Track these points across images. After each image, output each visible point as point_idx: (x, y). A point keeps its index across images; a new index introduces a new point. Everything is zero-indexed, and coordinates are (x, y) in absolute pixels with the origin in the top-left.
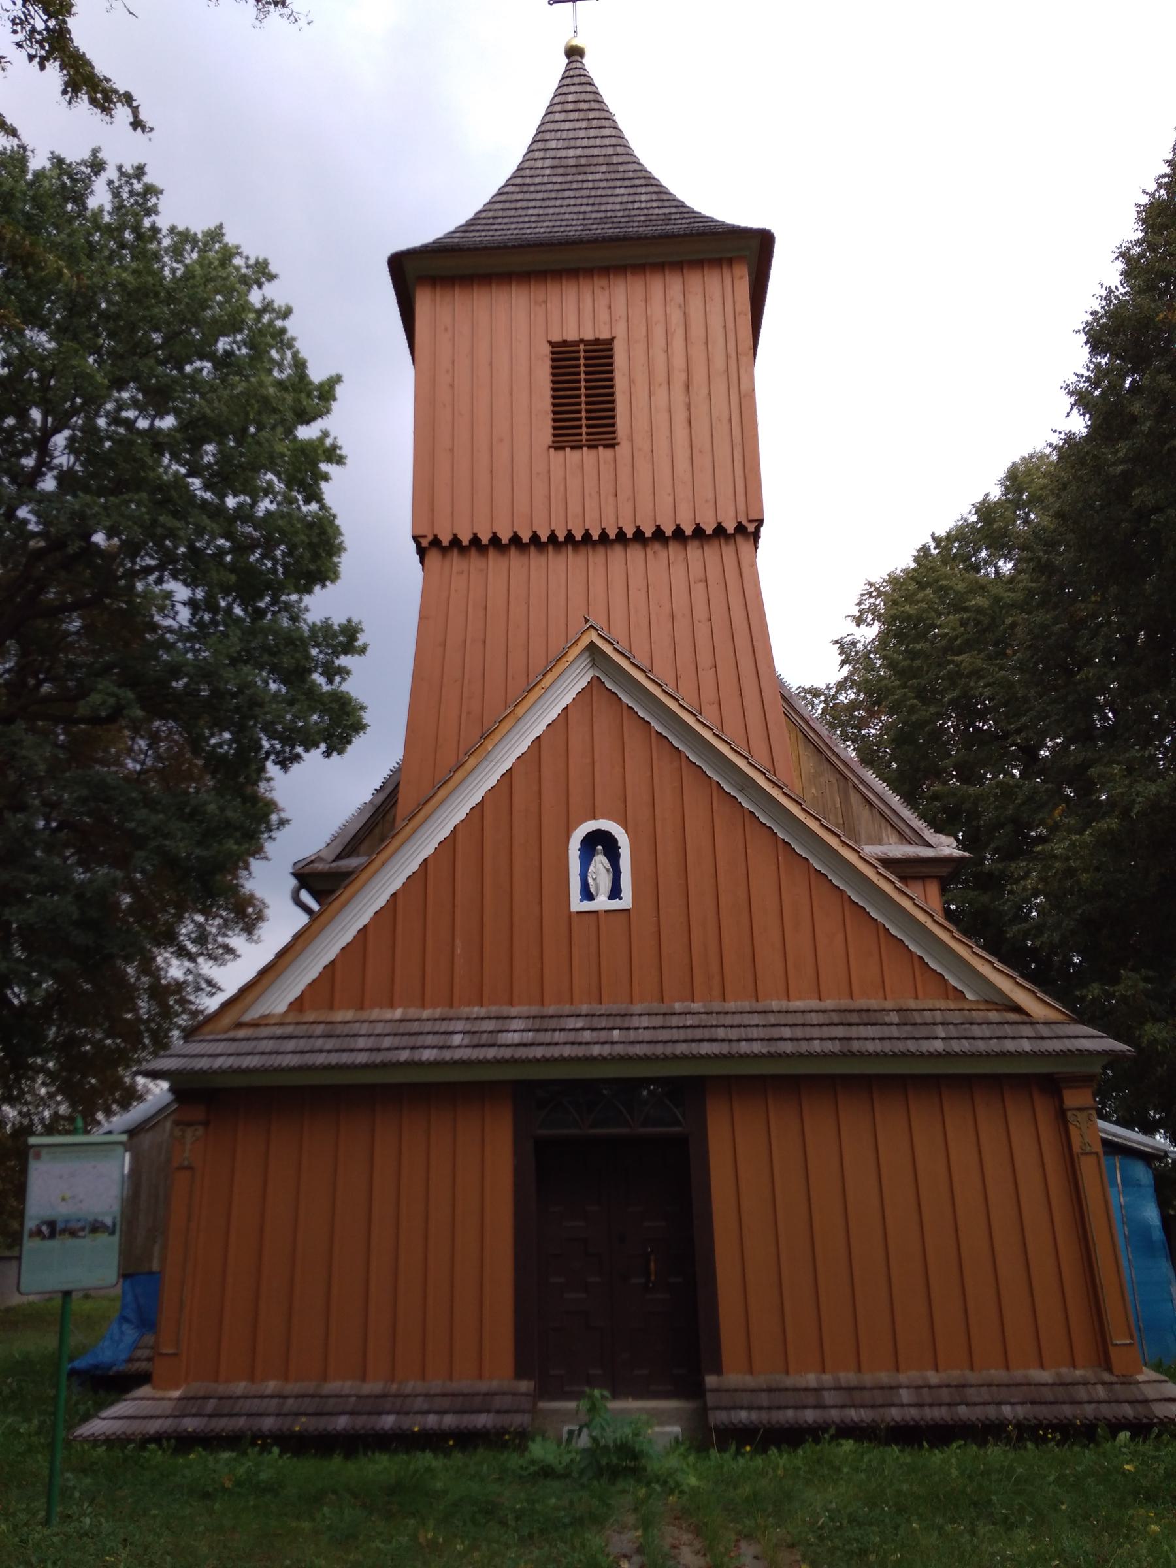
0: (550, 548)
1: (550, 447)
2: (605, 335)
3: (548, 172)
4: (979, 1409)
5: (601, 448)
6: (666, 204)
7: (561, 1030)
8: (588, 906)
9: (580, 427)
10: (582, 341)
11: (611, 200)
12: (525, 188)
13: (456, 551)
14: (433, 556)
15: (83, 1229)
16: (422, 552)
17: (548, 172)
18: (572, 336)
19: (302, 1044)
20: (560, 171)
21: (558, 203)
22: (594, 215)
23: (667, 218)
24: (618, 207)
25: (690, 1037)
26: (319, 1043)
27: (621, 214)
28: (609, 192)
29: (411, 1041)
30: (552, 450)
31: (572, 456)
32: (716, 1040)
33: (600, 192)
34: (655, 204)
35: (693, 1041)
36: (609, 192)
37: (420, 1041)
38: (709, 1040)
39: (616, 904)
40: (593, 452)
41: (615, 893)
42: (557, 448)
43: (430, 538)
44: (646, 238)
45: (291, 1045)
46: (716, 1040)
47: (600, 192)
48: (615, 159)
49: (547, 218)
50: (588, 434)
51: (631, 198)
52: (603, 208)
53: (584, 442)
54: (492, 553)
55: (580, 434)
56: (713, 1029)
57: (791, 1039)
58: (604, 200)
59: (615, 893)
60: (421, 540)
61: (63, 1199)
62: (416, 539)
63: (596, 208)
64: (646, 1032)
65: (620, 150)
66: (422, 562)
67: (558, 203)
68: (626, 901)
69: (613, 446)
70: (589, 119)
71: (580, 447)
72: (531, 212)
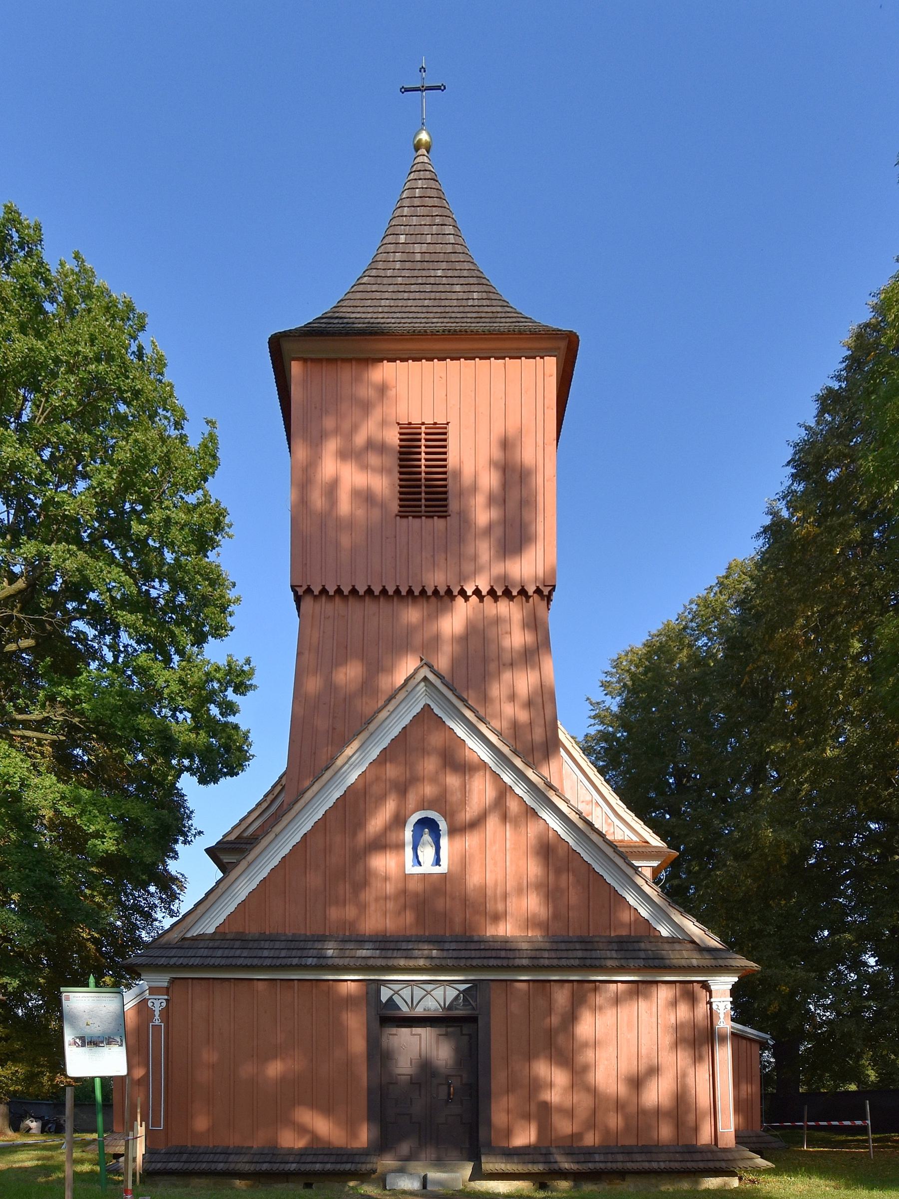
0: (395, 599)
1: (397, 515)
2: (441, 420)
3: (398, 265)
4: (638, 1164)
5: (436, 518)
6: (494, 303)
7: (398, 949)
8: (418, 870)
9: (420, 493)
10: (423, 424)
11: (449, 295)
12: (379, 280)
13: (324, 599)
14: (307, 602)
15: (102, 1042)
16: (298, 600)
17: (398, 265)
18: (416, 420)
19: (226, 953)
20: (408, 265)
21: (406, 295)
22: (435, 310)
23: (494, 316)
24: (455, 303)
25: (483, 956)
26: (238, 953)
27: (456, 309)
28: (448, 288)
29: (299, 953)
30: (398, 518)
31: (414, 523)
32: (500, 958)
33: (441, 288)
34: (485, 303)
35: (484, 958)
36: (448, 288)
37: (305, 953)
38: (495, 958)
39: (437, 870)
40: (430, 520)
41: (437, 862)
42: (401, 517)
43: (305, 588)
44: (477, 333)
45: (219, 953)
46: (500, 958)
47: (441, 288)
48: (453, 257)
49: (397, 310)
50: (426, 506)
51: (465, 296)
52: (443, 303)
53: (423, 513)
54: (351, 600)
55: (420, 500)
56: (498, 951)
57: (548, 958)
58: (443, 296)
59: (437, 862)
60: (297, 589)
61: (87, 1025)
62: (293, 588)
63: (436, 303)
64: (454, 952)
65: (459, 248)
66: (298, 609)
67: (406, 295)
68: (443, 868)
69: (445, 517)
70: (432, 216)
71: (420, 517)
72: (383, 303)
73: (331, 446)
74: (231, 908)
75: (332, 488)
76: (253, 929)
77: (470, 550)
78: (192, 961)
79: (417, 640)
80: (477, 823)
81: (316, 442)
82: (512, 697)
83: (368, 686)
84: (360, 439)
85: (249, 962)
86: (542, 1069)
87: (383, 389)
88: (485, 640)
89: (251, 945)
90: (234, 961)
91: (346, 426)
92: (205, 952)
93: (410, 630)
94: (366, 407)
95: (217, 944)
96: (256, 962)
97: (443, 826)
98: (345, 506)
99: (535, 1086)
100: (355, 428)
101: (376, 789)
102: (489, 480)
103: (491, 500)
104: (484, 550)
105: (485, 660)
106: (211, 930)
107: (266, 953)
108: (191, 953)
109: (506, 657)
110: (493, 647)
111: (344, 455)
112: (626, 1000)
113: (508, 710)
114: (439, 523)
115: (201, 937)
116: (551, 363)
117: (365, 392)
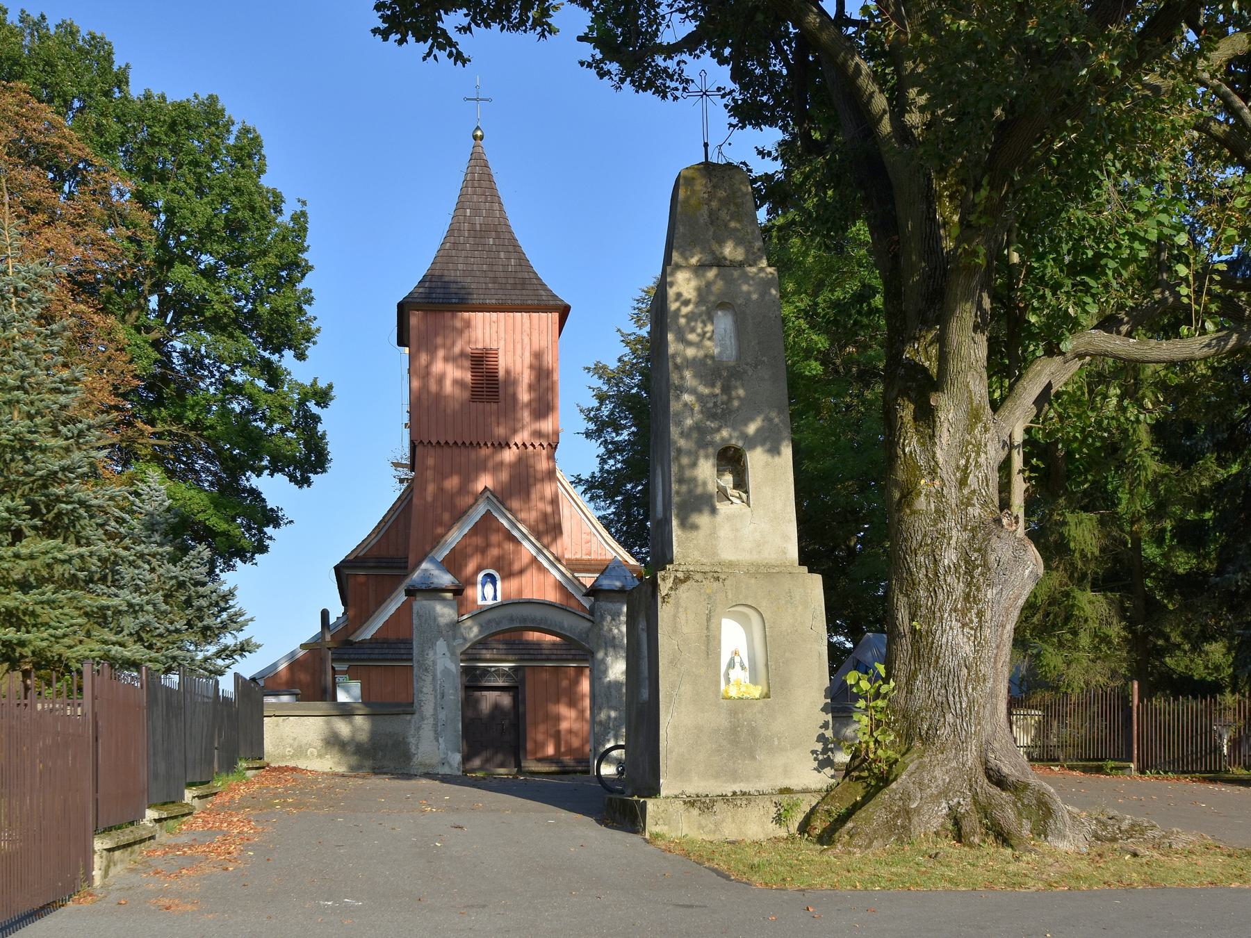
26: (387, 651)
31: (481, 405)
41: (495, 598)
45: (376, 651)
59: (495, 598)
73: (441, 353)
74: (380, 624)
75: (441, 379)
76: (392, 636)
77: (519, 415)
78: (363, 657)
79: (490, 464)
80: (521, 572)
81: (432, 352)
82: (542, 498)
83: (464, 489)
84: (457, 350)
85: (394, 657)
86: (564, 710)
87: (468, 324)
88: (527, 466)
89: (393, 646)
90: (385, 656)
91: (449, 342)
92: (369, 651)
93: (486, 459)
94: (460, 332)
95: (374, 646)
96: (398, 657)
97: (497, 576)
98: (448, 387)
99: (558, 718)
100: (453, 344)
101: (469, 550)
102: (526, 377)
103: (531, 387)
104: (526, 415)
105: (528, 477)
106: (369, 637)
107: (402, 651)
108: (361, 651)
109: (539, 476)
110: (531, 470)
111: (446, 359)
112: (408, 683)
113: (541, 505)
114: (494, 406)
115: (363, 641)
116: (556, 316)
117: (458, 324)
